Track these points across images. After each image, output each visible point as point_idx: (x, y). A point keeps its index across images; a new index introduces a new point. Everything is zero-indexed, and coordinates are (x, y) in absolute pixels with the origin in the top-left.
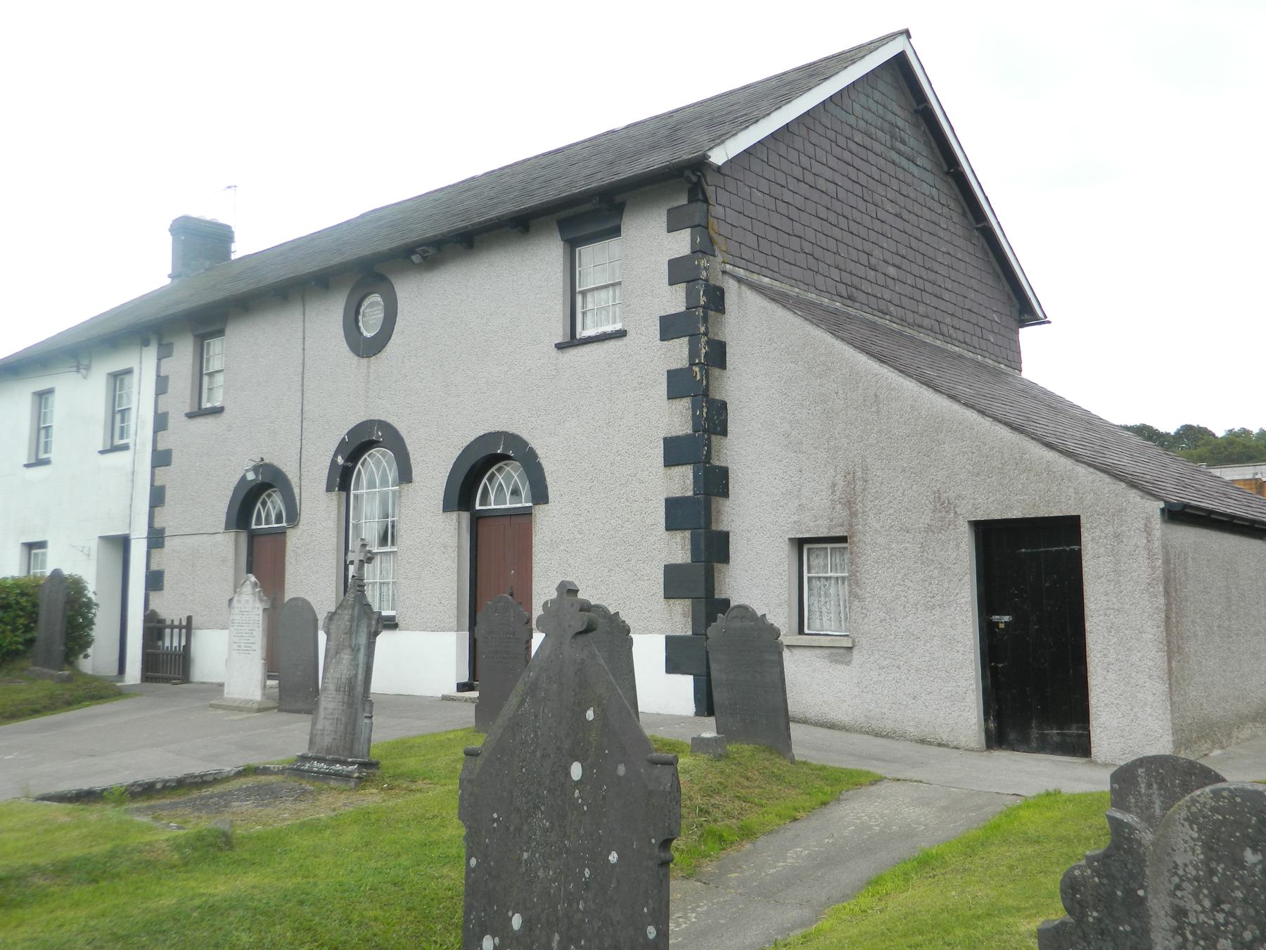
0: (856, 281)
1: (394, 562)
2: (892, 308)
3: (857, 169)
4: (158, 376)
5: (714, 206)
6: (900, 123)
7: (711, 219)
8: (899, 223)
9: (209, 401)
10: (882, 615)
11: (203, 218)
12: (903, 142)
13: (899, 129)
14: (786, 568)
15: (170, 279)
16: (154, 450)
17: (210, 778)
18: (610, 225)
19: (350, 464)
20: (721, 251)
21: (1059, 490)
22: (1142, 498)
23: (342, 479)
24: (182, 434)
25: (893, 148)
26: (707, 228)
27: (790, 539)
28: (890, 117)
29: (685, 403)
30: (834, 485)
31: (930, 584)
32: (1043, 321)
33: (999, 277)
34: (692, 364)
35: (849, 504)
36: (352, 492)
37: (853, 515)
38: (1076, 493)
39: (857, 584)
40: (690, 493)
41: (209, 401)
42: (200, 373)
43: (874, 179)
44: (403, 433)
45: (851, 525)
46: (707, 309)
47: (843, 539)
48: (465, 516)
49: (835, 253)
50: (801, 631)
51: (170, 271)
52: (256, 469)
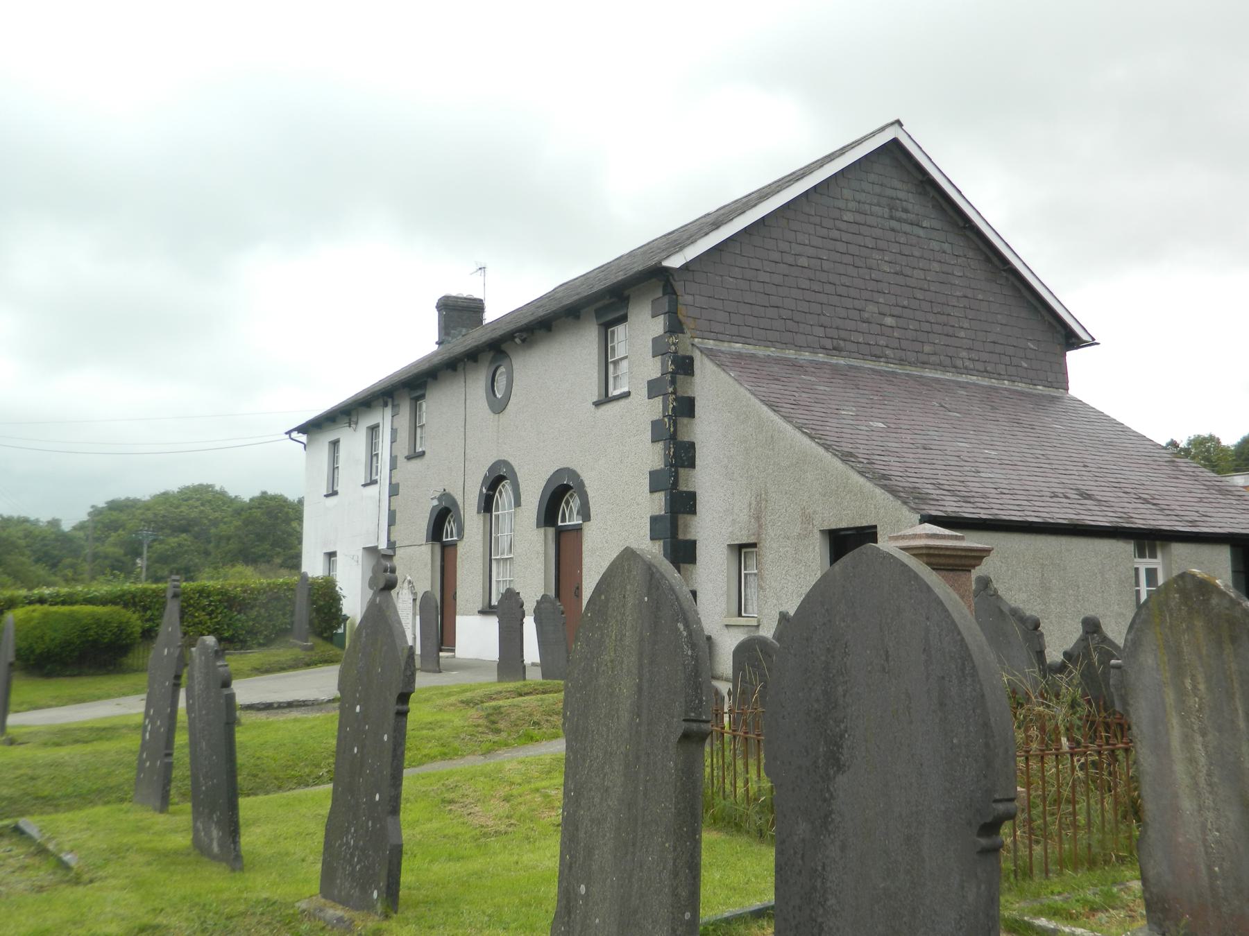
0: (843, 334)
1: (510, 566)
2: (888, 352)
3: (847, 243)
4: (392, 429)
5: (682, 296)
6: (901, 195)
7: (679, 306)
8: (900, 280)
9: (420, 447)
10: (775, 601)
11: (460, 296)
12: (906, 211)
13: (901, 200)
14: (726, 567)
15: (437, 346)
16: (390, 484)
17: (310, 703)
18: (622, 313)
19: (491, 493)
20: (688, 329)
21: (866, 506)
22: (909, 511)
23: (487, 504)
24: (409, 469)
25: (892, 218)
26: (676, 313)
27: (325, 553)
28: (890, 192)
29: (661, 445)
30: (750, 505)
31: (800, 578)
32: (1093, 343)
33: (1036, 308)
34: (664, 417)
35: (758, 519)
36: (494, 513)
37: (760, 526)
38: (875, 508)
39: (762, 579)
40: (663, 513)
41: (420, 447)
42: (415, 426)
43: (868, 247)
44: (516, 469)
45: (759, 535)
46: (676, 374)
47: (754, 545)
48: (551, 531)
49: (819, 315)
50: (740, 615)
51: (437, 340)
52: (440, 499)
